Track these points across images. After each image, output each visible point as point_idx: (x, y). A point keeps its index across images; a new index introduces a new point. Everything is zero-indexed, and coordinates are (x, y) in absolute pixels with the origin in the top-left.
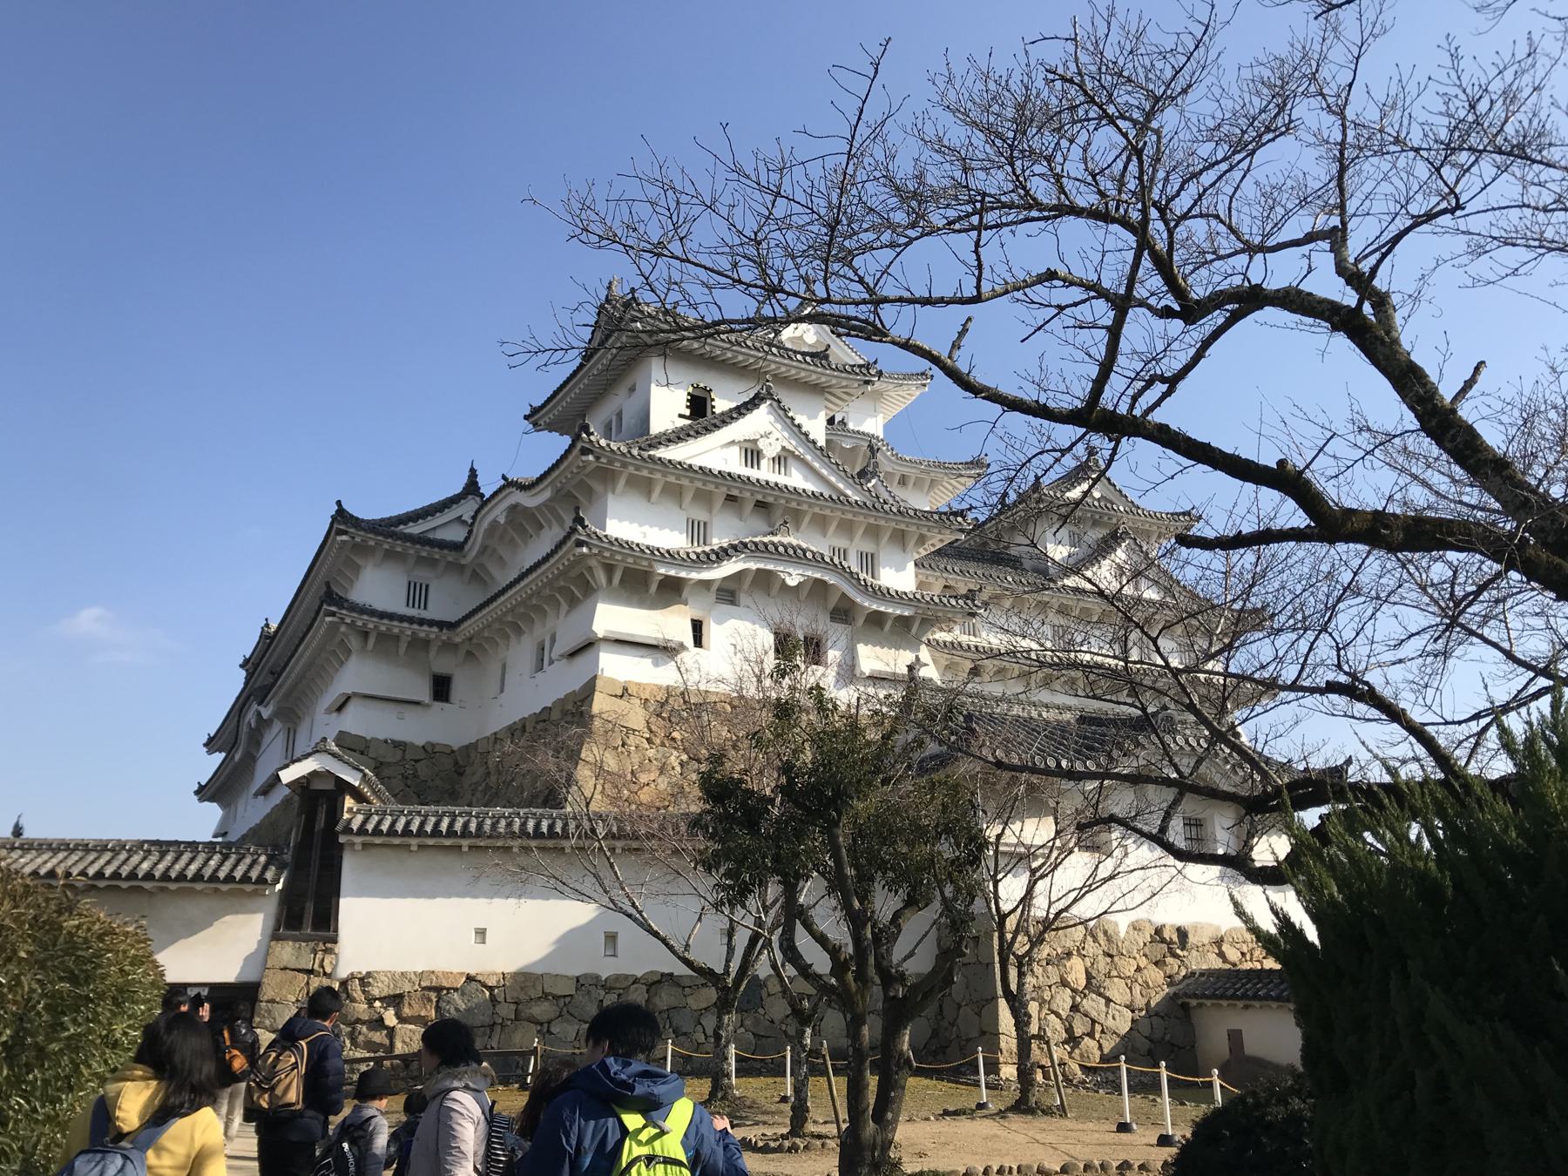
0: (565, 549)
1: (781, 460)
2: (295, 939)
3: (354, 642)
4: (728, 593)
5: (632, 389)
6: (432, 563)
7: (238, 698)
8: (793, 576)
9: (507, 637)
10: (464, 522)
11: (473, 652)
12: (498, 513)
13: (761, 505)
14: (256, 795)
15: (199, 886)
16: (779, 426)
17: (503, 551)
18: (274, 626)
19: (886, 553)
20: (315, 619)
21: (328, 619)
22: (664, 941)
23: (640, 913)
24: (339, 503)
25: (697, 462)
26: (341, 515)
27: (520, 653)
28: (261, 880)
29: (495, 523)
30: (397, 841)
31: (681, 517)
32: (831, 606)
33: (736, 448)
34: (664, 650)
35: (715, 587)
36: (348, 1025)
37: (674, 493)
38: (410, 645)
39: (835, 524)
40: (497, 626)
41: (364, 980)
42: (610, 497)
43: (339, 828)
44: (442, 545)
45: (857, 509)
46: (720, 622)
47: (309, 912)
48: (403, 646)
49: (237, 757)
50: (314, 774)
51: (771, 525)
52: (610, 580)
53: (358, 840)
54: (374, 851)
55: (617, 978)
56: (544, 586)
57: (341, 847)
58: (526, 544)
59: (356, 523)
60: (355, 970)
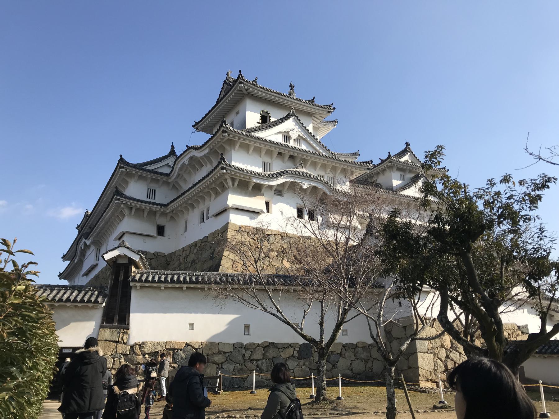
0: (216, 171)
1: (297, 140)
2: (111, 328)
3: (126, 212)
4: (279, 191)
5: (238, 113)
6: (156, 181)
7: (76, 239)
8: (306, 185)
9: (188, 210)
10: (170, 166)
11: (173, 217)
12: (185, 160)
13: (292, 157)
14: (83, 275)
15: (68, 304)
16: (297, 127)
17: (185, 176)
18: (90, 212)
19: (339, 176)
20: (110, 202)
21: (116, 201)
22: (292, 326)
23: (281, 313)
24: (121, 156)
25: (268, 138)
26: (122, 160)
27: (194, 216)
28: (96, 302)
29: (183, 164)
30: (155, 285)
31: (260, 161)
33: (280, 135)
34: (255, 213)
35: (274, 189)
36: (134, 365)
37: (258, 150)
38: (149, 213)
40: (184, 205)
41: (141, 346)
42: (233, 151)
43: (130, 279)
44: (161, 174)
45: (329, 159)
46: (275, 204)
47: (117, 316)
49: (76, 261)
50: (119, 256)
51: (295, 165)
52: (233, 185)
53: (138, 284)
54: (145, 290)
55: (251, 344)
56: (205, 188)
57: (131, 288)
58: (195, 173)
59: (128, 164)
60: (137, 341)
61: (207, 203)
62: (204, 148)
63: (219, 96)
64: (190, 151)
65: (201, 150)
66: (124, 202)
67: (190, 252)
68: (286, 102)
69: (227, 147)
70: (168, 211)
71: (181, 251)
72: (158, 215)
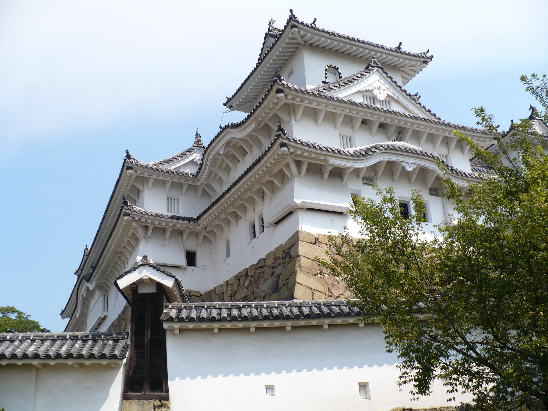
9: (229, 223)
10: (196, 163)
11: (208, 237)
12: (220, 148)
13: (382, 126)
15: (70, 362)
20: (117, 221)
21: (126, 218)
27: (239, 233)
32: (429, 187)
35: (362, 175)
37: (331, 118)
39: (425, 136)
40: (223, 216)
42: (293, 121)
48: (168, 234)
50: (141, 282)
52: (299, 172)
53: (177, 326)
61: (258, 208)
62: (248, 122)
63: (260, 55)
64: (225, 132)
65: (243, 127)
66: (137, 219)
67: (239, 285)
68: (361, 50)
69: (284, 116)
70: (199, 228)
71: (225, 287)
72: (185, 236)
